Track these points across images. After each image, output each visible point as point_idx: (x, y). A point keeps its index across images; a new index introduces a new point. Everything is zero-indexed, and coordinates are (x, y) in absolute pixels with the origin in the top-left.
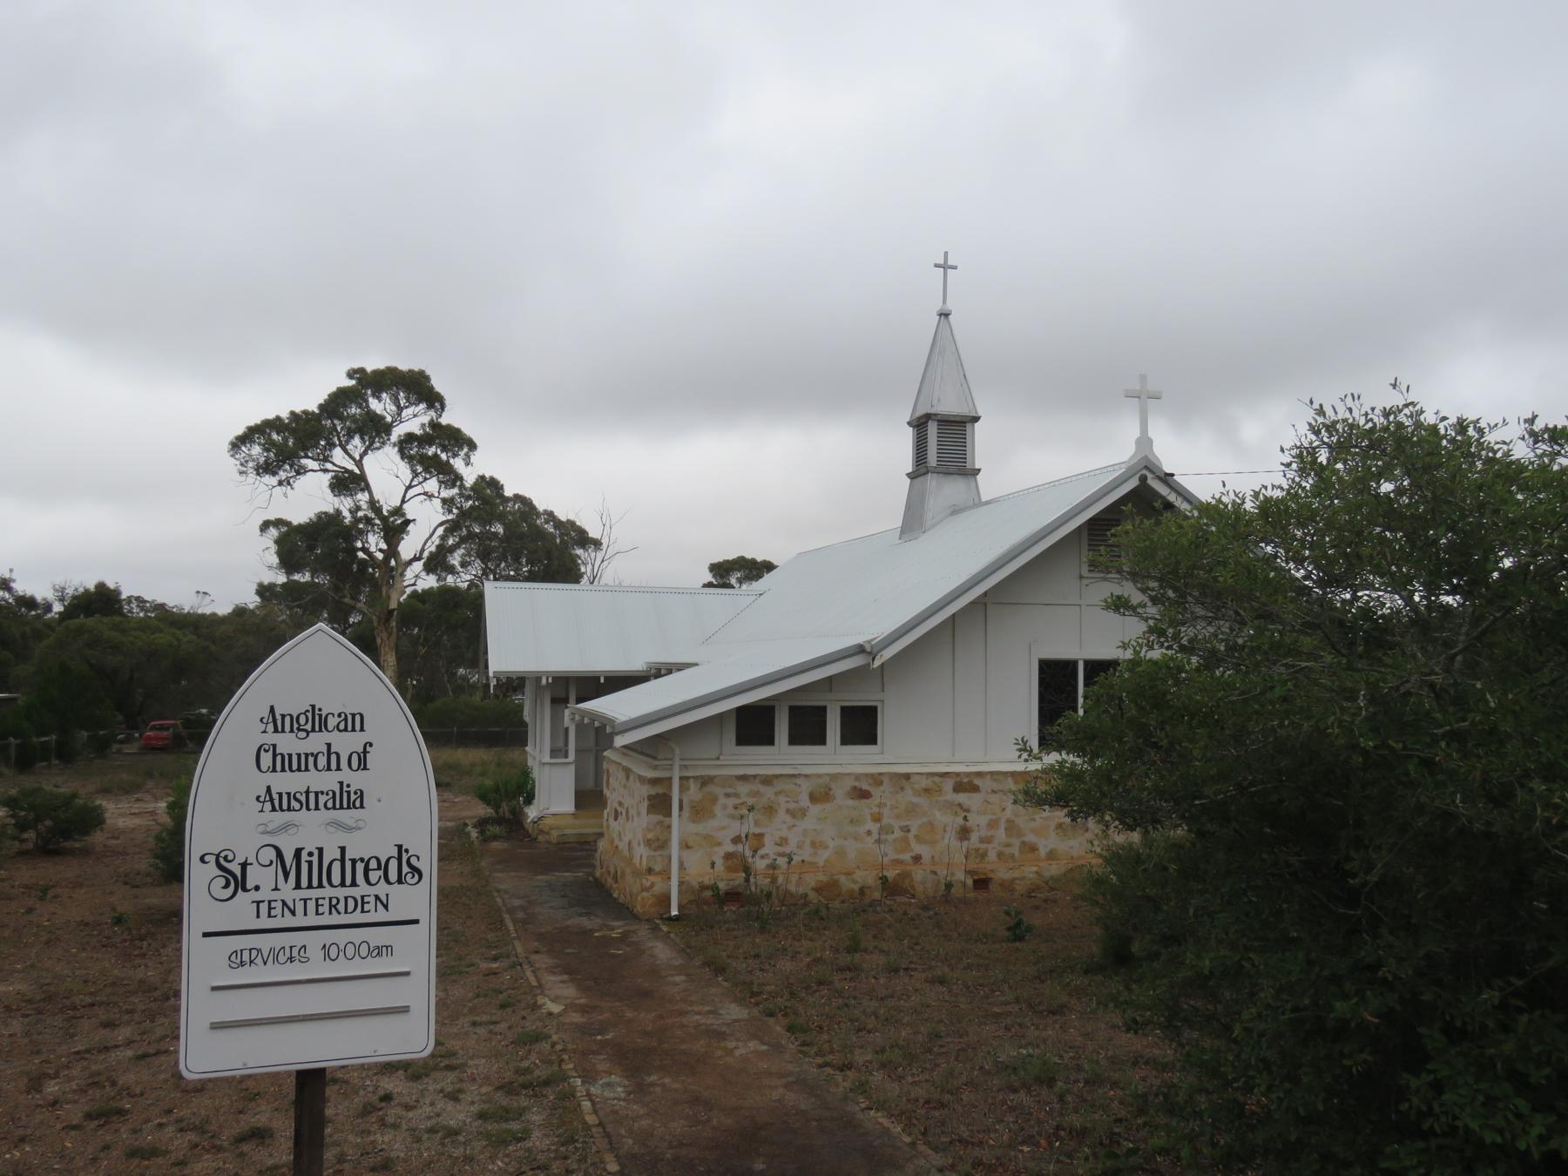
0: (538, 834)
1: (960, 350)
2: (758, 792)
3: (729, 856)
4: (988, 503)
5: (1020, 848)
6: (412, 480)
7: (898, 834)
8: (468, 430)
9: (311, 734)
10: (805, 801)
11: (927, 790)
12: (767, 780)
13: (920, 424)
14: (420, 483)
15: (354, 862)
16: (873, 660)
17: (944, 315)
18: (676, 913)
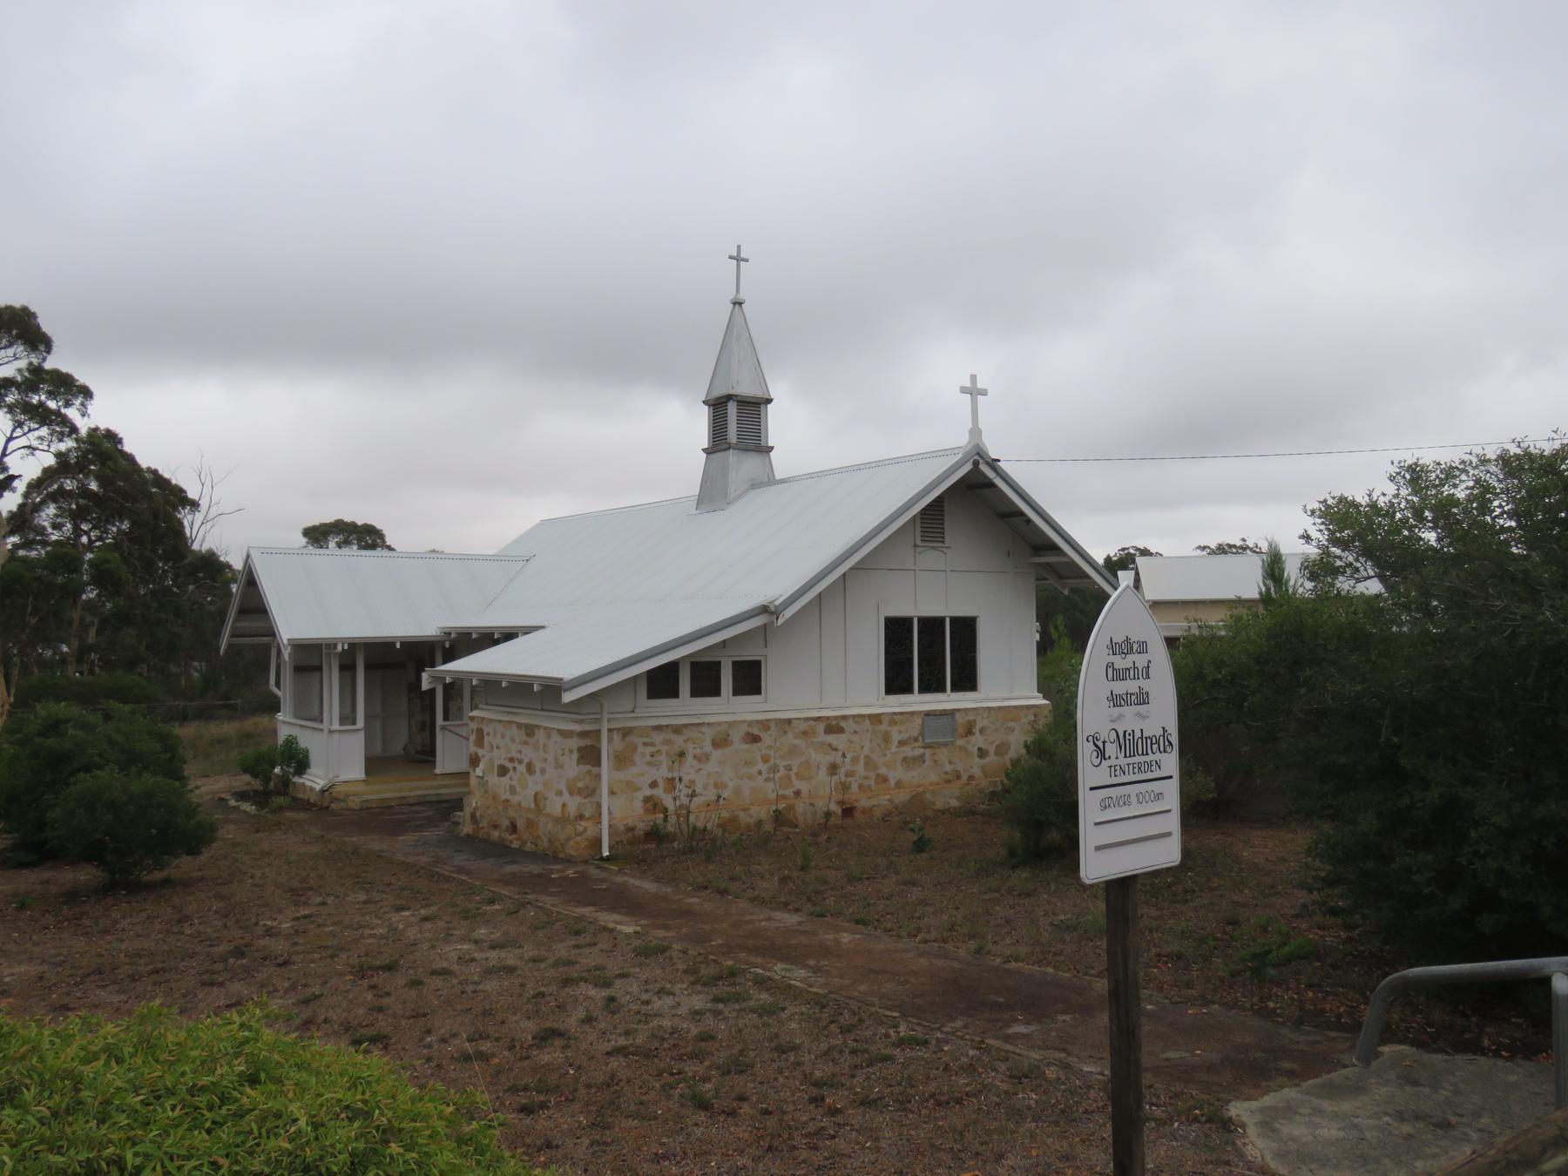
0: (331, 802)
1: (753, 335)
2: (670, 740)
3: (647, 799)
4: (783, 481)
5: (876, 779)
6: (13, 431)
7: (782, 772)
8: (82, 378)
9: (1128, 656)
10: (708, 747)
11: (805, 733)
12: (677, 730)
13: (718, 405)
14: (25, 434)
15: (1146, 738)
16: (777, 618)
17: (738, 303)
18: (608, 854)
